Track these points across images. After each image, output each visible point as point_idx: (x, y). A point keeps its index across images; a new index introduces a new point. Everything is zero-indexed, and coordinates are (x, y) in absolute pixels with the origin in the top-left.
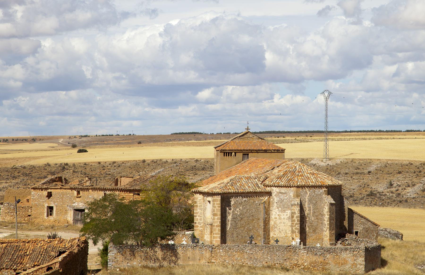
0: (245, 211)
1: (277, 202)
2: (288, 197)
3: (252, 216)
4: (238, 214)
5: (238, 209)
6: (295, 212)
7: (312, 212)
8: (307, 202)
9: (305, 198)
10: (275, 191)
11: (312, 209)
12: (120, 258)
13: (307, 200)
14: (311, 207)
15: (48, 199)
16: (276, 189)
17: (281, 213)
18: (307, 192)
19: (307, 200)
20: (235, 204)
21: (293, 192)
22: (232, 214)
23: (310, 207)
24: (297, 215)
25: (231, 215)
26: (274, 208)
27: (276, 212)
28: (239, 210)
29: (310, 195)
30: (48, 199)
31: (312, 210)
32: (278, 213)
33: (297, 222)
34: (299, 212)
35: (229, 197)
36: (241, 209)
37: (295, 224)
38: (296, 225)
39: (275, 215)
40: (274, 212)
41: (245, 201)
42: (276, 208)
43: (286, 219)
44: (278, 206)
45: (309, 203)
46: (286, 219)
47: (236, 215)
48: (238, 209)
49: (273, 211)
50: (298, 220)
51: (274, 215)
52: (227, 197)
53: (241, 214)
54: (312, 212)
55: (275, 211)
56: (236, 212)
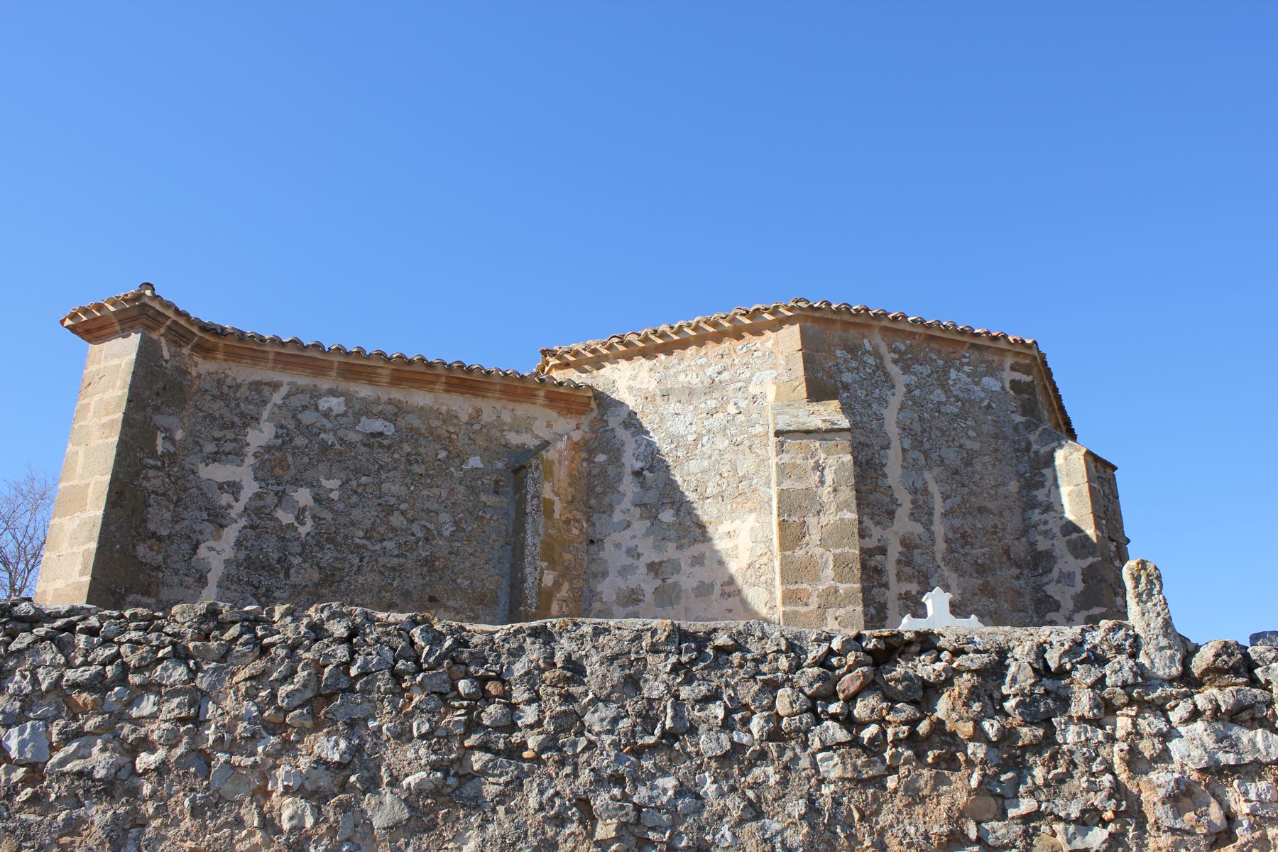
0: (365, 515)
1: (638, 465)
2: (732, 409)
3: (429, 562)
4: (303, 530)
5: (303, 496)
6: (809, 494)
7: (939, 528)
8: (896, 445)
9: (880, 419)
10: (630, 388)
11: (939, 507)
12: (1106, 626)
13: (892, 430)
14: (934, 489)
15: (570, 655)
16: (634, 378)
17: (671, 551)
18: (886, 374)
19: (892, 430)
20: (279, 449)
21: (774, 367)
22: (243, 522)
23: (925, 491)
24: (829, 518)
25: (231, 533)
26: (617, 517)
27: (632, 544)
28: (317, 499)
29: (913, 400)
30: (570, 655)
31: (944, 515)
32: (651, 556)
33: (841, 578)
34: (848, 494)
35: (239, 386)
36: (335, 495)
37: (814, 602)
38: (830, 613)
39: (625, 571)
40: (618, 546)
41: (373, 435)
42: (637, 512)
43: (717, 589)
44: (651, 497)
45: (915, 454)
46: (717, 589)
47: (283, 536)
48: (303, 496)
49: (608, 544)
50: (840, 562)
51: (612, 575)
52: (220, 383)
53: (323, 537)
54: (939, 528)
55: (624, 537)
56: (285, 517)
